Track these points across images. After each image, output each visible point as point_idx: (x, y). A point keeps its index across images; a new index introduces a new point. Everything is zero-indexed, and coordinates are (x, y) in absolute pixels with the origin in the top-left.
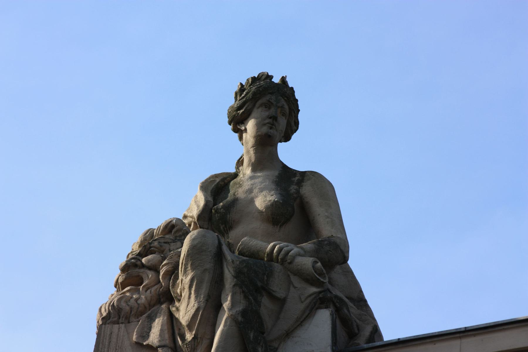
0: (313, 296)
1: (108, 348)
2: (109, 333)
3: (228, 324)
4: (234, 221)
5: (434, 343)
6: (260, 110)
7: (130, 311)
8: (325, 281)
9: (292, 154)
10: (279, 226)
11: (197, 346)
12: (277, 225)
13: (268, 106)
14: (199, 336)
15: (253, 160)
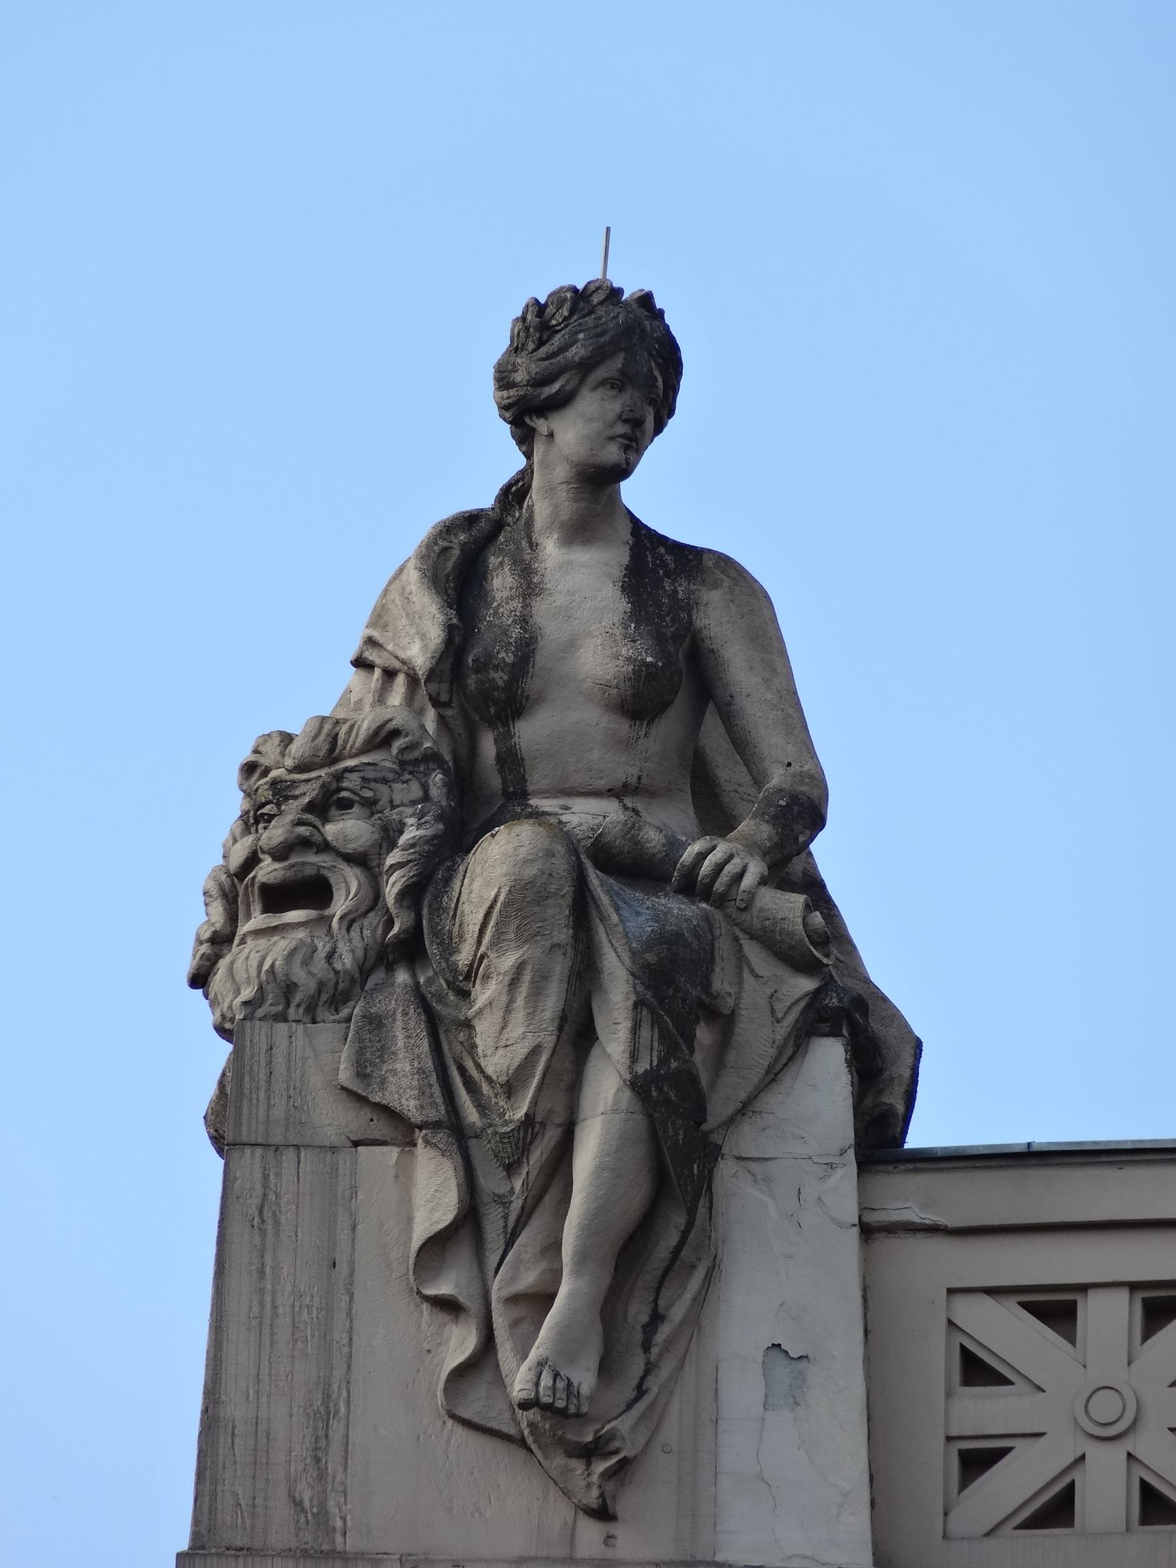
0: (803, 1004)
1: (268, 1090)
2: (264, 1047)
4: (528, 698)
5: (1120, 1165)
8: (825, 961)
9: (662, 492)
10: (645, 722)
11: (531, 1142)
12: (642, 720)
13: (617, 384)
14: (539, 1118)
15: (565, 516)
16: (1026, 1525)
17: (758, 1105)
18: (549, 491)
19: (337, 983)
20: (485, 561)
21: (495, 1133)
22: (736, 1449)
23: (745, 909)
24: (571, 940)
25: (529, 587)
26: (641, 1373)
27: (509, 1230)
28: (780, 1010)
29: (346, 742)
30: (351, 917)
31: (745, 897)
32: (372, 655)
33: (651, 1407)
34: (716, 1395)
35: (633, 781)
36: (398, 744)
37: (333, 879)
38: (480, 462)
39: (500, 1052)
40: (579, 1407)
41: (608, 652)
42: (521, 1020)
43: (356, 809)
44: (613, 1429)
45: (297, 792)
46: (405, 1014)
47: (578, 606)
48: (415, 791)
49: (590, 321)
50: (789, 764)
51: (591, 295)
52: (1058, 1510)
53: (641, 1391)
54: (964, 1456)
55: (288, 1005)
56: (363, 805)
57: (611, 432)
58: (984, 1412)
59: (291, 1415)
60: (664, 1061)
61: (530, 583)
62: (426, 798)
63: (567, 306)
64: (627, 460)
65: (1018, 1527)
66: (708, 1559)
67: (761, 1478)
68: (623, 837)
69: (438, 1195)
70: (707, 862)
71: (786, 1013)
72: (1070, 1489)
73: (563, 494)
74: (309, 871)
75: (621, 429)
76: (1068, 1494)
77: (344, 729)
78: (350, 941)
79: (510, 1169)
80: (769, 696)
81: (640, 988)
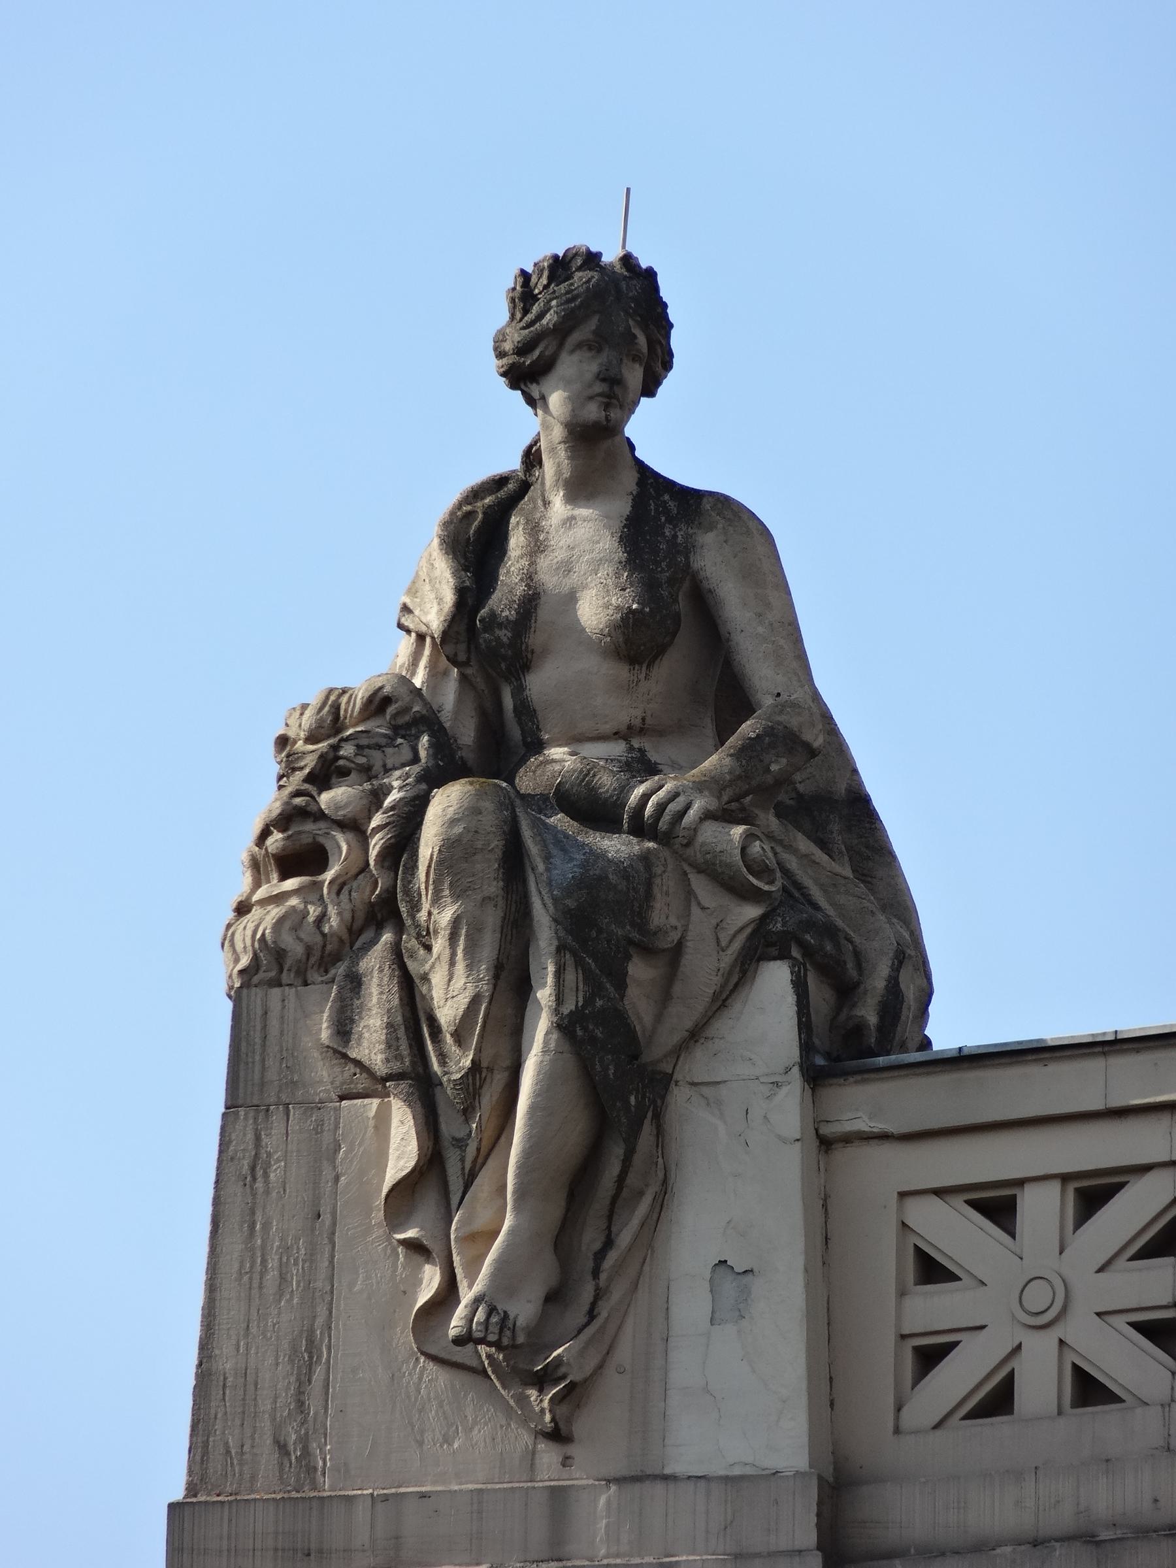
0: (749, 930)
2: (259, 1012)
3: (552, 1046)
4: (533, 652)
6: (576, 357)
7: (304, 958)
9: (666, 434)
11: (481, 1087)
12: (640, 664)
13: (595, 345)
14: (484, 1064)
15: (567, 474)
16: (972, 1415)
17: (711, 1031)
18: (553, 450)
19: (324, 946)
20: (508, 522)
21: (449, 1080)
22: (684, 1366)
23: (687, 845)
24: (501, 892)
25: (536, 545)
26: (592, 1299)
27: (467, 1171)
28: (724, 938)
29: (346, 711)
30: (341, 880)
31: (686, 833)
32: (407, 622)
33: (602, 1330)
34: (667, 1313)
35: (637, 722)
36: (391, 710)
37: (328, 845)
38: (503, 430)
39: (449, 1003)
40: (514, 1337)
41: (600, 602)
42: (462, 972)
43: (353, 775)
44: (559, 1355)
45: (302, 764)
46: (381, 970)
47: (576, 557)
48: (406, 754)
49: (563, 288)
50: (779, 695)
51: (570, 261)
52: (998, 1400)
53: (592, 1315)
54: (918, 1350)
55: (281, 971)
56: (360, 771)
57: (590, 392)
58: (933, 1309)
59: (277, 1364)
60: (589, 1001)
61: (537, 540)
62: (416, 759)
63: (546, 274)
64: (607, 417)
65: (965, 1418)
66: (657, 1472)
67: (706, 1390)
68: (580, 784)
69: (404, 1143)
70: (650, 803)
71: (731, 941)
72: (1010, 1379)
73: (562, 453)
74: (306, 840)
75: (599, 388)
76: (1008, 1384)
77: (344, 699)
78: (338, 904)
79: (467, 1113)
80: (760, 630)
81: (562, 934)
